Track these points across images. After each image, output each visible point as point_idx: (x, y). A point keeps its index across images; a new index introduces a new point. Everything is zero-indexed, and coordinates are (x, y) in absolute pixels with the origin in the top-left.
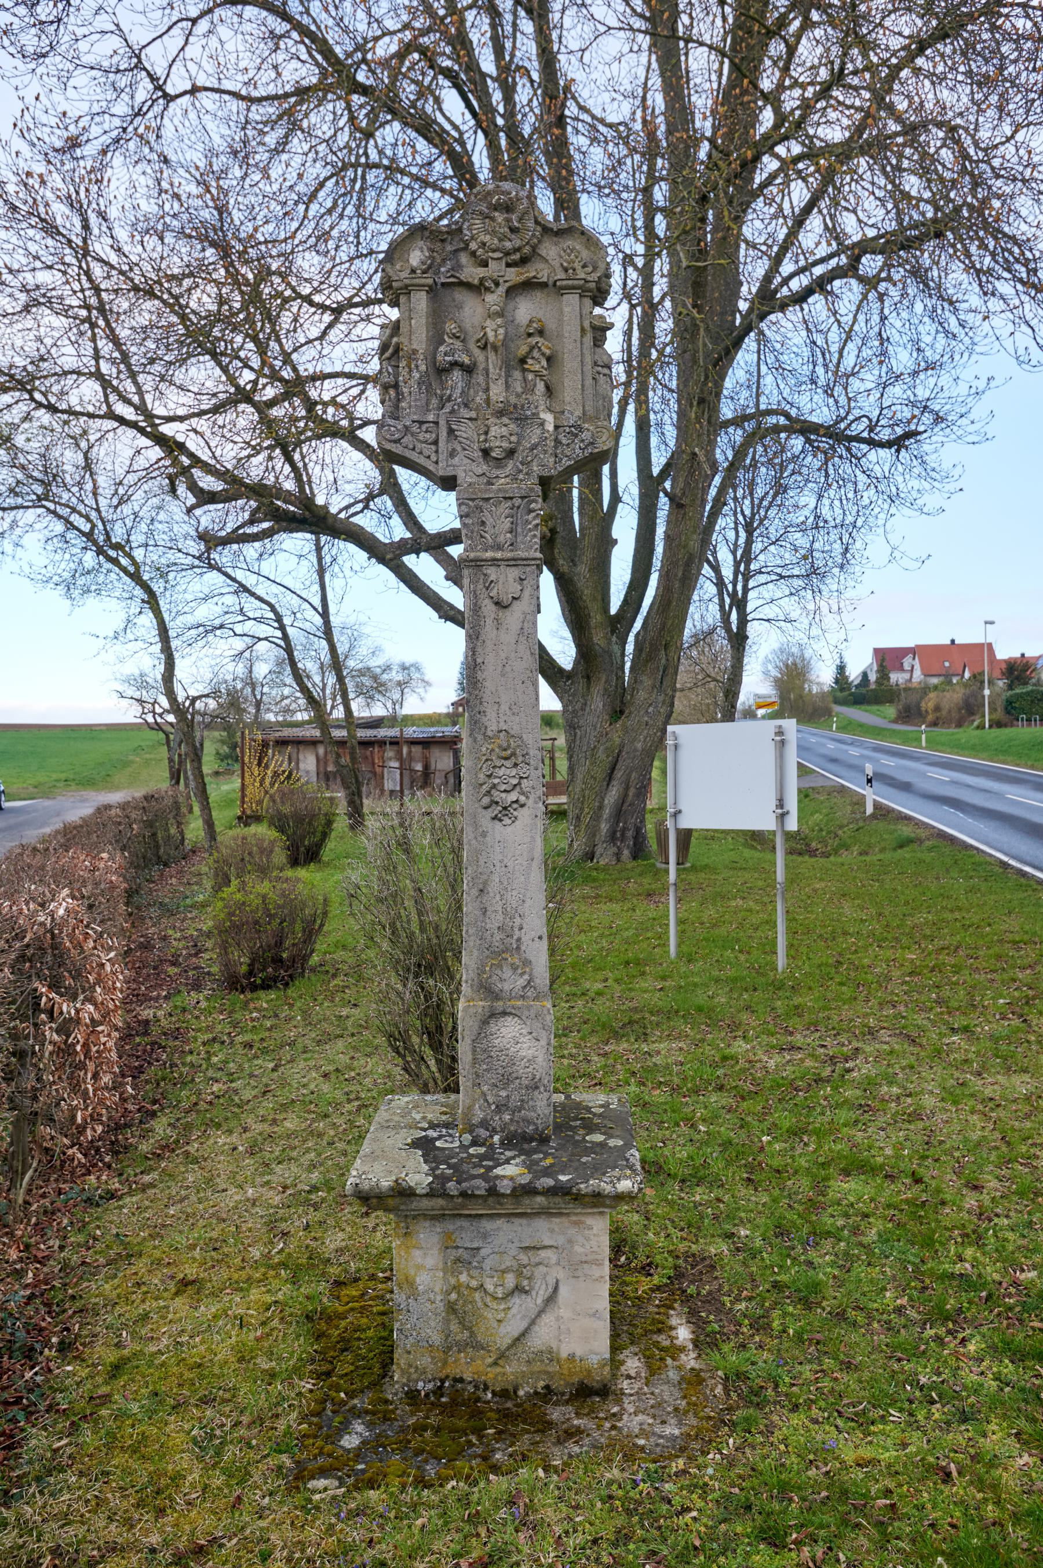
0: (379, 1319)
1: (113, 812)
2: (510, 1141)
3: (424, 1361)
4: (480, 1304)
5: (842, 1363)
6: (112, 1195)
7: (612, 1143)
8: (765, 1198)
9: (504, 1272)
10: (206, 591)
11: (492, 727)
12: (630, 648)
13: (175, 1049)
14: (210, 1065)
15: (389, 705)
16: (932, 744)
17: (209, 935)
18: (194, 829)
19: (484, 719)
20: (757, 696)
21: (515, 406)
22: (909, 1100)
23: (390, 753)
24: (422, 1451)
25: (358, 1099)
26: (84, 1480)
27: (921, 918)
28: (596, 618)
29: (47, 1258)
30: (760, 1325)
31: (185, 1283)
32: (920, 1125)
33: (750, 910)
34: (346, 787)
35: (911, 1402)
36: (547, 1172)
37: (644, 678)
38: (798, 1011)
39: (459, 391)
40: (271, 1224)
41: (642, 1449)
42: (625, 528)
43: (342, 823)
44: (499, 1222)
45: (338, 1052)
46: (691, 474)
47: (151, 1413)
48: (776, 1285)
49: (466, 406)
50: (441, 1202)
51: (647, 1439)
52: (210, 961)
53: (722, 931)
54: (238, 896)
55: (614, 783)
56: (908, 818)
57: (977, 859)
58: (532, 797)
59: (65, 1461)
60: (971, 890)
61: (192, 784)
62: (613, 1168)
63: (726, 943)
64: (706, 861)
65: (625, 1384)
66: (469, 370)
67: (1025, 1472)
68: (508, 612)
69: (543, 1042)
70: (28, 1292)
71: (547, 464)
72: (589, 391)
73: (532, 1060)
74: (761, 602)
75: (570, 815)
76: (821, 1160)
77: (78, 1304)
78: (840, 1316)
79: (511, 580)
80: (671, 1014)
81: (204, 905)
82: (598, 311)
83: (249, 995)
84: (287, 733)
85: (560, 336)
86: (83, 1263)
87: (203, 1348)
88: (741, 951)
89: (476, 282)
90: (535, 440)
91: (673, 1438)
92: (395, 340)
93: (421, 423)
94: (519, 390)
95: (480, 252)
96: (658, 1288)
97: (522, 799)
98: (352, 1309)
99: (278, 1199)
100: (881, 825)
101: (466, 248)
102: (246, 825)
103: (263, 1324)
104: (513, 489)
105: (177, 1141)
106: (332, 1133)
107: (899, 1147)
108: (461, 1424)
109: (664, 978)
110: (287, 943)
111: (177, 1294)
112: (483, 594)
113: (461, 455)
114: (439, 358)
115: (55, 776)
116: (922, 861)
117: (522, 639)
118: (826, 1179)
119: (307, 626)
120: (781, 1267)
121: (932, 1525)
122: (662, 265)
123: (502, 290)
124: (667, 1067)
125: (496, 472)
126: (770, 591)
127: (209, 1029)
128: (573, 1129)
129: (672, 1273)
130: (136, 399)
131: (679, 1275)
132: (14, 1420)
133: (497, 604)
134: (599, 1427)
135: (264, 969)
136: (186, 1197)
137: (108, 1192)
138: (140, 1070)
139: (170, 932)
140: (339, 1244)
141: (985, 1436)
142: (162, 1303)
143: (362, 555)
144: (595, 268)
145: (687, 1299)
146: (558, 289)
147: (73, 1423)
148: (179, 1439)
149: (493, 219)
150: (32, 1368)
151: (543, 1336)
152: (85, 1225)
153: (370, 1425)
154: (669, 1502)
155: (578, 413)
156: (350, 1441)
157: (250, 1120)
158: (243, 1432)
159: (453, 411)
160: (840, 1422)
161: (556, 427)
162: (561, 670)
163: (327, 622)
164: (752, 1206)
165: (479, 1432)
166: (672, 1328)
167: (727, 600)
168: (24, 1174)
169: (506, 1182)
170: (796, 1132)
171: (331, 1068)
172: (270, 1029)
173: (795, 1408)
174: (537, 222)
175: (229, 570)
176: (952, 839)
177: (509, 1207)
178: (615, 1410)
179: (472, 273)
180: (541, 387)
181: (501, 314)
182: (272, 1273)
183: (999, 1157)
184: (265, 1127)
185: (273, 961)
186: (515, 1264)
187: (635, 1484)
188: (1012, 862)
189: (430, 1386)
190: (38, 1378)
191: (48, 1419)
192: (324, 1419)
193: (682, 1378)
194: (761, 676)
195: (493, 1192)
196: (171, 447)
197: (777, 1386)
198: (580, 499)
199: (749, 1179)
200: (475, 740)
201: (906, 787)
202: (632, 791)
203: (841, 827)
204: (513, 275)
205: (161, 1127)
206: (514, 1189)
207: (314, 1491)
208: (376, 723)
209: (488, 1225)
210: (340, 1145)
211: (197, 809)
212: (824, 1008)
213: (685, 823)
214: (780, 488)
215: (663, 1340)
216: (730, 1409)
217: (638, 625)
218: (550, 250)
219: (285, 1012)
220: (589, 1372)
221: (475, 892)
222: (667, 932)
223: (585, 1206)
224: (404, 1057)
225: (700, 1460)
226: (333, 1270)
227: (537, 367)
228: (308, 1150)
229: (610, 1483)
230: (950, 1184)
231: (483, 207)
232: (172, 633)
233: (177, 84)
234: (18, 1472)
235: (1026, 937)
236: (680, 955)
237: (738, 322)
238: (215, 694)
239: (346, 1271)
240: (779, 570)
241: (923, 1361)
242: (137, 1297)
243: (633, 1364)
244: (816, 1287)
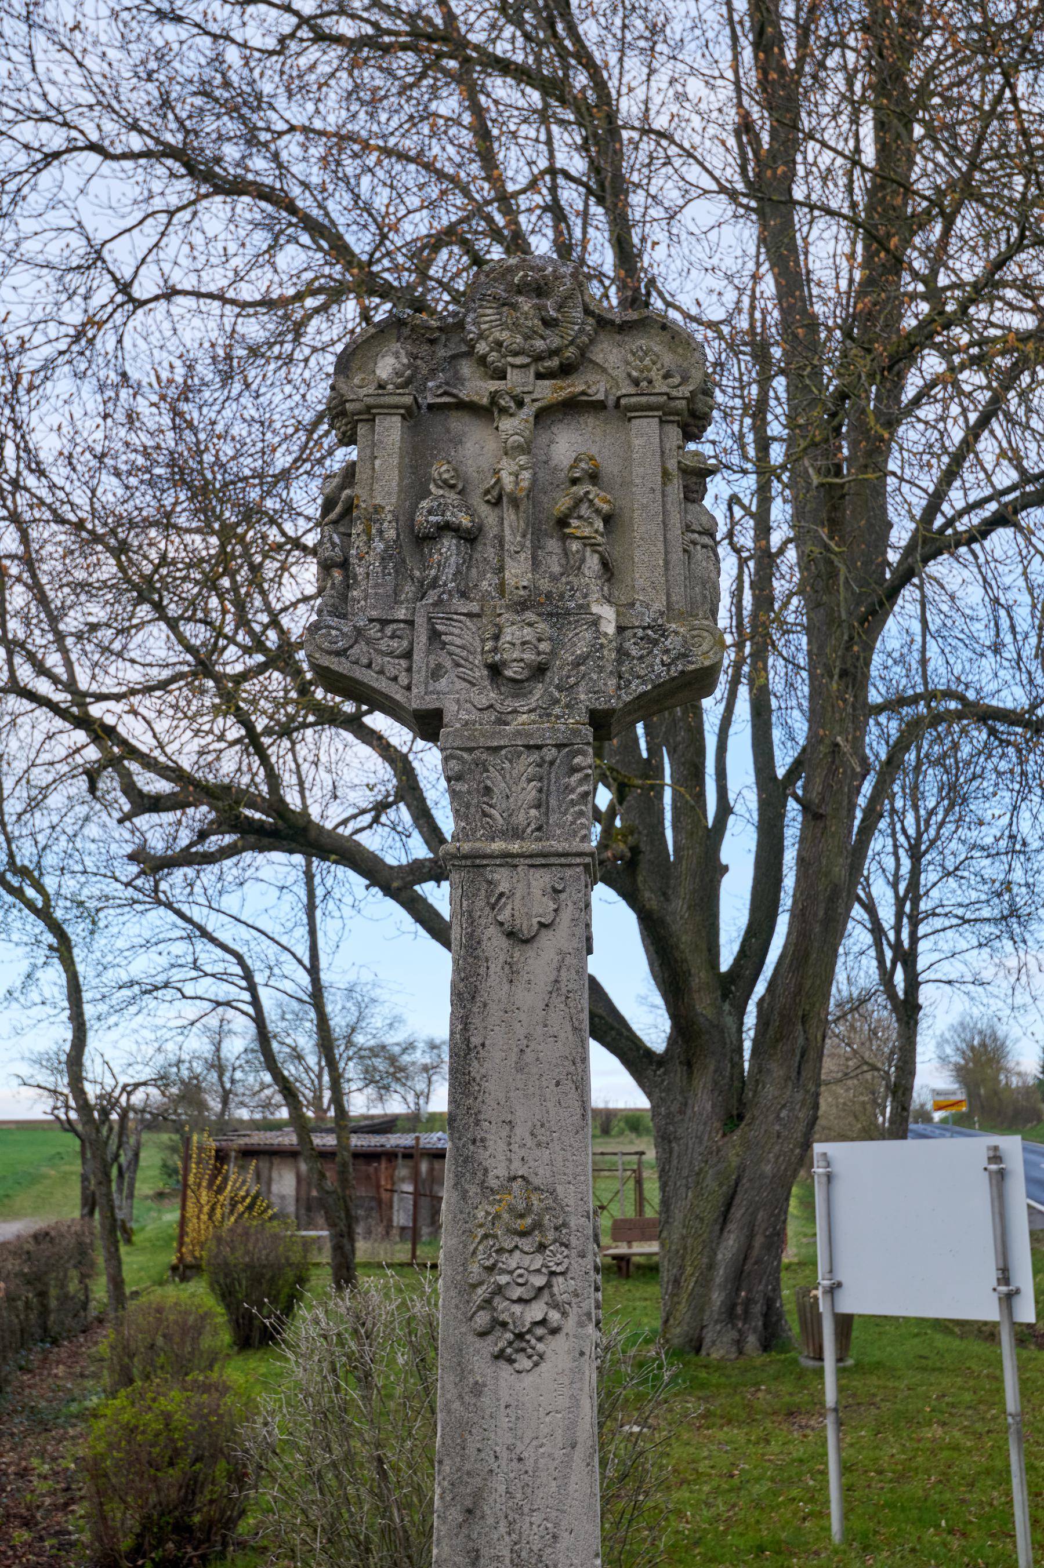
10: (147, 934)
11: (498, 1171)
12: (750, 1019)
15: (411, 1098)
19: (483, 1155)
20: (937, 1093)
21: (549, 596)
23: (403, 1171)
28: (699, 977)
33: (956, 1448)
34: (332, 1225)
37: (774, 1066)
39: (451, 571)
42: (739, 849)
43: (322, 1279)
46: (832, 772)
49: (464, 595)
53: (915, 1488)
55: (732, 1226)
58: (574, 1313)
66: (470, 537)
68: (530, 951)
71: (607, 691)
72: (678, 571)
74: (936, 956)
75: (665, 1275)
79: (537, 892)
82: (692, 446)
84: (259, 1138)
85: (627, 484)
88: (951, 1532)
89: (485, 401)
90: (581, 649)
92: (347, 492)
93: (384, 622)
94: (556, 569)
95: (493, 356)
97: (554, 1316)
101: (470, 353)
102: (184, 1279)
104: (545, 732)
110: (200, 1500)
112: (485, 916)
113: (452, 675)
114: (419, 518)
117: (557, 1001)
119: (288, 986)
122: (780, 511)
123: (528, 412)
125: (511, 704)
126: (951, 940)
130: (60, 671)
133: (511, 935)
135: (161, 1542)
139: (35, 1462)
143: (358, 881)
144: (685, 380)
146: (621, 412)
149: (514, 307)
155: (659, 605)
159: (439, 603)
161: (621, 629)
162: (649, 1053)
163: (316, 981)
167: (889, 954)
174: (587, 312)
175: (185, 908)
179: (477, 387)
180: (593, 562)
181: (525, 449)
194: (936, 1063)
196: (102, 733)
198: (674, 807)
200: (464, 1196)
202: (759, 1241)
204: (547, 391)
208: (387, 1125)
213: (848, 1305)
214: (954, 796)
217: (760, 988)
218: (610, 354)
221: (455, 1515)
222: (824, 1488)
227: (587, 531)
231: (500, 290)
232: (86, 996)
233: (145, 287)
237: (888, 576)
238: (162, 1080)
240: (960, 912)
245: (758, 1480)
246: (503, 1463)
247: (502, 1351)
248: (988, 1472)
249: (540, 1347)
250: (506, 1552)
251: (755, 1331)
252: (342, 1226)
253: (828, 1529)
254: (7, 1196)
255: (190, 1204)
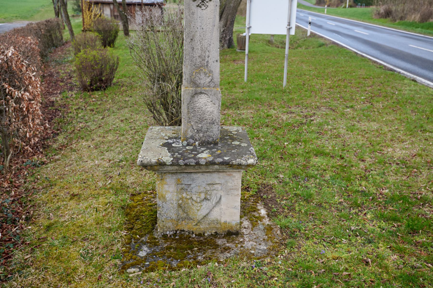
0: (150, 208)
1: (34, 25)
2: (202, 144)
3: (170, 224)
4: (190, 204)
5: (323, 222)
6: (43, 163)
7: (243, 145)
8: (288, 164)
9: (200, 193)
13: (65, 111)
14: (78, 117)
16: (328, 13)
17: (74, 72)
18: (66, 35)
22: (335, 131)
24: (170, 257)
25: (134, 129)
26: (37, 271)
27: (330, 70)
29: (19, 186)
30: (291, 209)
31: (73, 196)
32: (341, 139)
33: (271, 66)
35: (349, 236)
36: (219, 156)
38: (292, 100)
40: (105, 174)
41: (253, 254)
43: (121, 34)
44: (199, 175)
45: (126, 113)
47: (63, 245)
48: (295, 194)
50: (176, 167)
51: (255, 250)
52: (75, 81)
54: (84, 56)
55: (222, 19)
56: (322, 37)
57: (347, 51)
59: (30, 263)
60: (346, 61)
61: (64, 18)
62: (246, 154)
63: (264, 77)
64: (253, 50)
65: (244, 230)
67: (394, 261)
69: (217, 105)
70: (12, 199)
73: (212, 112)
76: (307, 151)
77: (32, 203)
78: (320, 205)
80: (247, 101)
81: (72, 61)
83: (91, 93)
86: (33, 188)
87: (82, 220)
88: (269, 80)
91: (265, 250)
96: (252, 196)
98: (139, 204)
99: (107, 165)
100: (313, 39)
103: (105, 210)
105: (67, 144)
106: (126, 141)
107: (334, 147)
108: (184, 246)
109: (243, 88)
111: (71, 199)
115: (12, 15)
116: (328, 51)
118: (309, 157)
120: (296, 188)
121: (364, 281)
124: (247, 118)
127: (77, 104)
128: (226, 139)
129: (257, 190)
131: (260, 191)
132: (8, 247)
134: (236, 246)
135: (96, 84)
136: (72, 164)
137: (42, 162)
138: (52, 119)
140: (132, 181)
141: (378, 248)
142: (65, 203)
145: (263, 200)
147: (32, 249)
148: (75, 254)
150: (15, 227)
151: (215, 215)
152: (33, 174)
153: (150, 247)
154: (266, 274)
156: (142, 254)
157: (95, 137)
158: (100, 251)
160: (325, 244)
164: (283, 167)
165: (191, 249)
166: (259, 210)
168: (7, 155)
169: (203, 160)
170: (296, 142)
171: (124, 118)
172: (100, 105)
173: (308, 238)
176: (337, 44)
177: (204, 169)
178: (241, 240)
182: (107, 191)
183: (370, 150)
184: (101, 139)
185: (99, 80)
186: (204, 190)
187: (253, 268)
188: (359, 52)
189: (172, 233)
190: (18, 231)
191: (22, 247)
192: (132, 246)
193: (265, 228)
195: (198, 164)
197: (300, 231)
199: (281, 157)
201: (320, 27)
202: (229, 23)
203: (299, 40)
205: (61, 139)
206: (206, 163)
207: (131, 273)
209: (194, 176)
210: (129, 145)
211: (67, 28)
212: (301, 99)
215: (255, 214)
216: (284, 239)
219: (105, 99)
220: (232, 227)
221: (189, 40)
223: (234, 169)
224: (153, 113)
225: (276, 258)
226: (131, 190)
228: (117, 147)
229: (244, 268)
230: (354, 160)
234: (11, 268)
235: (368, 77)
236: (248, 80)
239: (135, 190)
241: (352, 221)
242: (55, 200)
243: (246, 223)
244: (310, 196)
245: (228, 72)
246: (199, 29)
247: (199, 5)
248: (277, 70)
249: (207, 4)
250: (200, 48)
251: (226, 43)
252: (125, 20)
253: (244, 80)
254: (32, 15)
255: (84, 14)
